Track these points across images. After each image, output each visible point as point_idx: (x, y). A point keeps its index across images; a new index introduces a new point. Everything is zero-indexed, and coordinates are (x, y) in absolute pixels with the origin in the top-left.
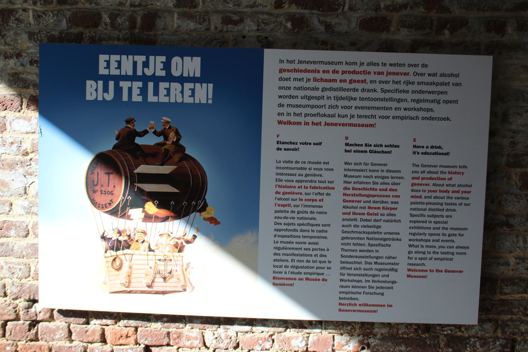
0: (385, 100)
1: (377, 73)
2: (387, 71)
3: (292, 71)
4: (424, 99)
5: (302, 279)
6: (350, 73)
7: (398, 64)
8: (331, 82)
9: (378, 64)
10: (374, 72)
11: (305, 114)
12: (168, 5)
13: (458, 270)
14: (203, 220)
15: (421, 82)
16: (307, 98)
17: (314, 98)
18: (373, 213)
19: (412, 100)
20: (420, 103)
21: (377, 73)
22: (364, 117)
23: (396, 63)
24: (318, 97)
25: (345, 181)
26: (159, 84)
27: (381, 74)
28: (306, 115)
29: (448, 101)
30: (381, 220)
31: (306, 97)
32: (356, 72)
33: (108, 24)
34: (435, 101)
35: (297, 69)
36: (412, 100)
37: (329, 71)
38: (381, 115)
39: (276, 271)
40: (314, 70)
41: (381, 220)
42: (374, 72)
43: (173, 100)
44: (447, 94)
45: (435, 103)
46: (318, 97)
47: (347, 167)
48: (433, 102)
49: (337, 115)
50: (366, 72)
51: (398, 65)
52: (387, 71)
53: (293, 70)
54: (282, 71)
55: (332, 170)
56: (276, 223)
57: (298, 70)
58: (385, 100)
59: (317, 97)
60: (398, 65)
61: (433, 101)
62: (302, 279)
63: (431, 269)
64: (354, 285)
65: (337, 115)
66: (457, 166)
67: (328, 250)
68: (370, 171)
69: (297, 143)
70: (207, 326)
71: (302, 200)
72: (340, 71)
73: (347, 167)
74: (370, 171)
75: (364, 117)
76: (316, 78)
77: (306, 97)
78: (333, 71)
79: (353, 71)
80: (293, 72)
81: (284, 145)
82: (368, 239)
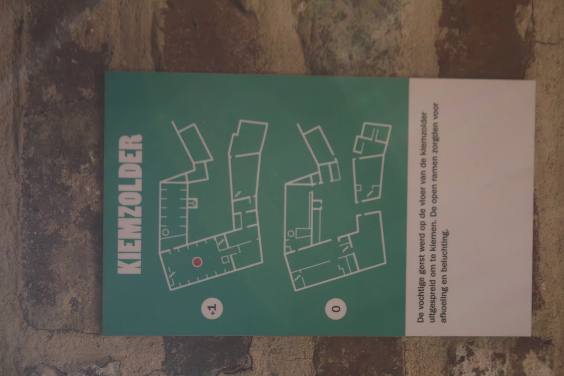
1: (423, 180)
5: (434, 209)
9: (436, 117)
11: (418, 322)
16: (433, 313)
17: (433, 303)
18: (431, 287)
22: (422, 239)
24: (431, 298)
26: (119, 275)
28: (433, 282)
29: (433, 195)
31: (432, 316)
33: (288, 244)
39: (432, 174)
42: (422, 183)
43: (140, 147)
44: (431, 322)
46: (431, 298)
47: (426, 318)
55: (436, 106)
57: (432, 286)
59: (432, 299)
62: (434, 209)
63: (431, 258)
64: (430, 248)
66: (432, 266)
68: (433, 250)
69: (437, 152)
71: (433, 257)
72: (432, 254)
73: (426, 318)
75: (433, 292)
77: (432, 316)
79: (436, 195)
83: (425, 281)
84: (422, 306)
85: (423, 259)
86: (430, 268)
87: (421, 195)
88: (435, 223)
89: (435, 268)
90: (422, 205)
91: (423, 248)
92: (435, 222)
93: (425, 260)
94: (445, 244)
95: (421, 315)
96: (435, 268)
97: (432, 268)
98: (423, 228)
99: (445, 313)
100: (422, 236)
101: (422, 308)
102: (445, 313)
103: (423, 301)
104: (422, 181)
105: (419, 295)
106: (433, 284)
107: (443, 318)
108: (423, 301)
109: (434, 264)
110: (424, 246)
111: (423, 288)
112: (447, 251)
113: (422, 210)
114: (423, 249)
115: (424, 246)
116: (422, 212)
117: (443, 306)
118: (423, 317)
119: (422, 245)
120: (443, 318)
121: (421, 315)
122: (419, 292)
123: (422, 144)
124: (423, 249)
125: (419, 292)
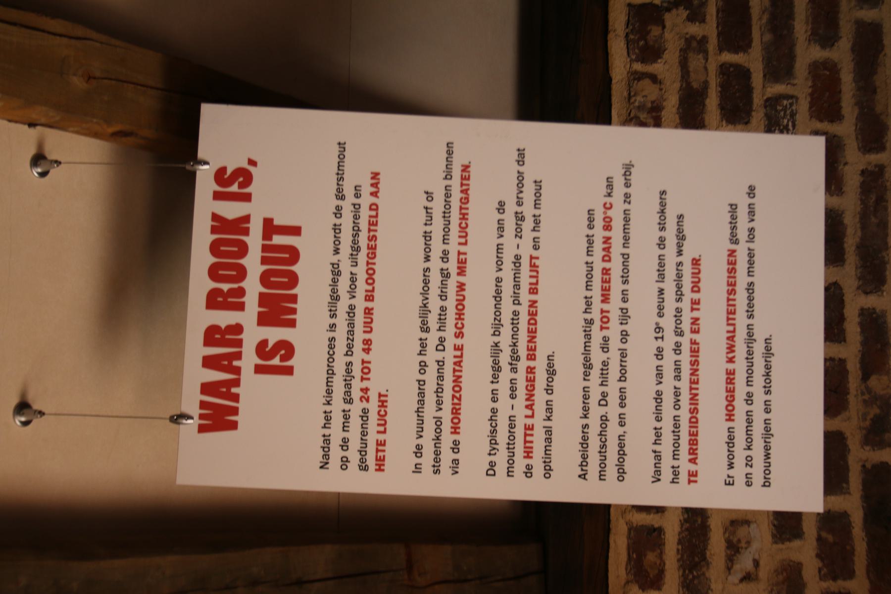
0: (438, 464)
2: (327, 331)
4: (583, 354)
10: (749, 222)
12: (633, 69)
19: (586, 378)
20: (591, 362)
22: (731, 449)
30: (426, 208)
34: (588, 329)
36: (586, 378)
38: (434, 406)
41: (426, 208)
45: (590, 331)
48: (590, 335)
49: (548, 423)
52: (327, 331)
56: (491, 472)
58: (436, 464)
61: (587, 335)
62: (456, 443)
65: (548, 423)
68: (749, 448)
70: (610, 28)
74: (749, 448)
76: (601, 344)
82: (327, 463)
83: (690, 415)
87: (676, 289)
88: (770, 339)
90: (350, 298)
91: (769, 454)
94: (548, 460)
95: (492, 465)
98: (624, 340)
99: (770, 374)
100: (606, 258)
101: (501, 270)
102: (770, 374)
103: (626, 375)
104: (749, 218)
105: (599, 435)
108: (626, 375)
110: (769, 452)
111: (590, 327)
112: (607, 437)
113: (661, 237)
114: (733, 349)
115: (769, 452)
116: (662, 241)
118: (607, 398)
119: (679, 246)
121: (492, 465)
123: (677, 272)
124: (733, 349)
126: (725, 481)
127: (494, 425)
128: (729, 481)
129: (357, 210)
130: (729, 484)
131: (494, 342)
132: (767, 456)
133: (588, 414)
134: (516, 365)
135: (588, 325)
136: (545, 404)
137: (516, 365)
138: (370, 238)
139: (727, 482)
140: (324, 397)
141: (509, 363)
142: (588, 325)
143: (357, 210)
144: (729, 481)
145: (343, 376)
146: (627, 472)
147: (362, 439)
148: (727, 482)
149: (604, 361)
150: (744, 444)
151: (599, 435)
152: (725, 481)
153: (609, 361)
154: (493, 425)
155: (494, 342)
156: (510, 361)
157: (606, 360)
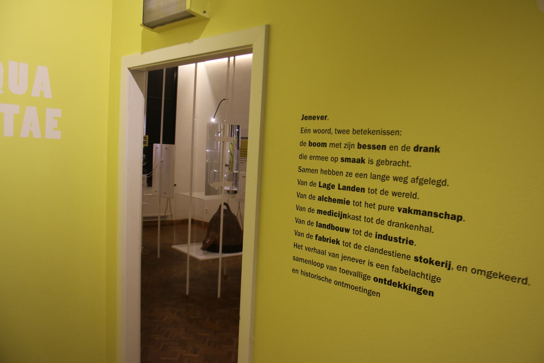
1: (402, 210)
3: (442, 216)
6: (337, 228)
7: (362, 130)
8: (425, 215)
13: (320, 114)
14: (420, 210)
15: (346, 158)
21: (402, 210)
22: (405, 195)
23: (360, 130)
25: (296, 244)
27: (428, 215)
32: (389, 237)
35: (343, 200)
37: (385, 146)
40: (433, 148)
42: (398, 208)
50: (410, 287)
51: (363, 131)
53: (443, 214)
54: (422, 292)
57: (344, 201)
60: (363, 131)
67: (369, 158)
75: (405, 195)
78: (415, 147)
79: (384, 236)
80: (400, 165)
81: (427, 217)
84: (358, 262)
85: (344, 160)
86: (325, 142)
89: (481, 274)
92: (432, 232)
93: (370, 144)
96: (481, 274)
97: (482, 271)
105: (446, 213)
106: (356, 131)
107: (416, 180)
109: (467, 271)
114: (396, 180)
117: (316, 146)
120: (416, 180)
122: (425, 274)
124: (396, 180)
125: (425, 274)
126: (303, 128)
127: (419, 275)
128: (303, 130)
129: (412, 197)
130: (302, 130)
131: (439, 148)
132: (314, 118)
133: (503, 279)
134: (417, 182)
135: (431, 278)
136: (396, 145)
137: (417, 182)
138: (436, 214)
139: (302, 129)
140: (407, 238)
141: (394, 266)
142: (431, 278)
143: (412, 197)
144: (303, 130)
145: (430, 274)
146: (445, 178)
147: (389, 207)
148: (302, 129)
149: (413, 242)
150: (326, 135)
151: (446, 213)
152: (303, 128)
153: (414, 245)
154: (418, 274)
155: (439, 148)
156: (419, 178)
157: (414, 244)
